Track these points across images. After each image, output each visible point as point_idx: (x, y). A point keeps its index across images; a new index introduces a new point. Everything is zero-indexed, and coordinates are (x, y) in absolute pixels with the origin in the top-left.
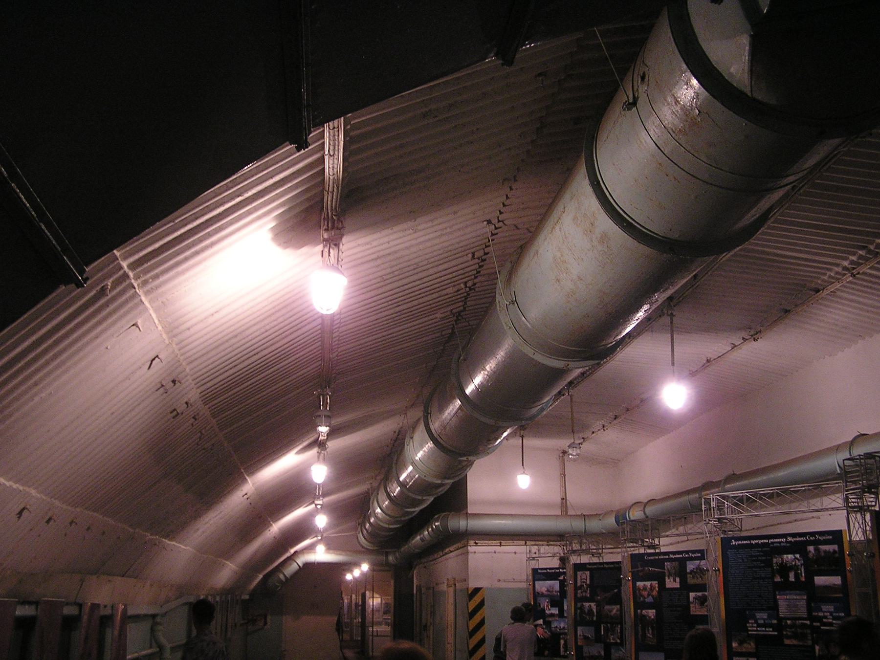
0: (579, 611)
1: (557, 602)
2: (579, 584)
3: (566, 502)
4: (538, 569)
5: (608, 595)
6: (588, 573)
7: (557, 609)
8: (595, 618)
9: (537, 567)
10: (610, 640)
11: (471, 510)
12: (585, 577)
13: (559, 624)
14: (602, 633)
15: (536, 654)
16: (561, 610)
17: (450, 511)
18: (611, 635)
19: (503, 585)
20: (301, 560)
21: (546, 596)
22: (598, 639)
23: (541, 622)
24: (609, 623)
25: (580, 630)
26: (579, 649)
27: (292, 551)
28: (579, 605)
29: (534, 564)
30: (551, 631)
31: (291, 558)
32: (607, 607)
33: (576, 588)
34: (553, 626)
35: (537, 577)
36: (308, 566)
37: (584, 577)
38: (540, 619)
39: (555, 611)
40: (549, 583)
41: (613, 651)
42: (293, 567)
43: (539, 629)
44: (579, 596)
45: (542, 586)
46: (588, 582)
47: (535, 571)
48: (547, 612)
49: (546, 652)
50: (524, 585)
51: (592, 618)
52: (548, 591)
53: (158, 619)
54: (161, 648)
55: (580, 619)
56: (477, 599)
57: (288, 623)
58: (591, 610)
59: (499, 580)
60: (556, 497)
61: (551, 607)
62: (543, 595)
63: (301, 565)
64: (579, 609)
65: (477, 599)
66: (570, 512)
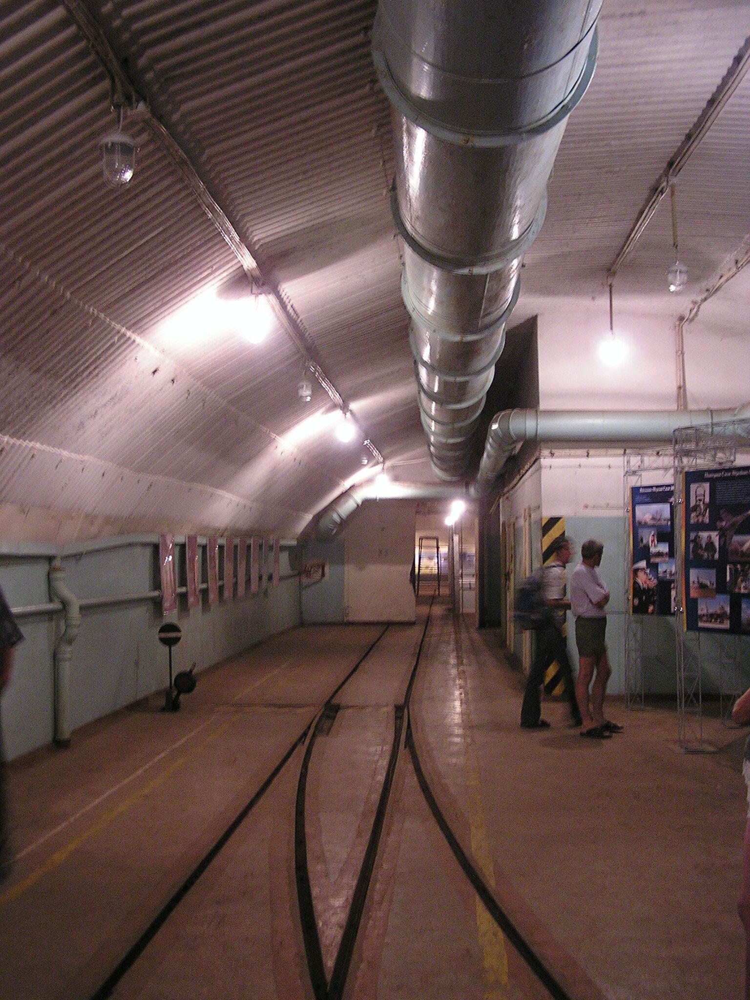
0: (692, 545)
1: (665, 535)
2: (693, 503)
3: (685, 390)
4: (640, 488)
5: (739, 519)
6: (707, 486)
7: (667, 545)
8: (717, 556)
9: (638, 485)
10: (740, 589)
11: (543, 405)
12: (702, 491)
13: (668, 567)
14: (728, 578)
15: (636, 610)
16: (671, 547)
17: (513, 408)
18: (742, 581)
19: (590, 513)
20: (359, 496)
21: (652, 526)
22: (722, 587)
23: (643, 564)
24: (739, 563)
25: (694, 574)
26: (692, 605)
27: (346, 484)
28: (692, 536)
29: (634, 481)
30: (658, 578)
31: (345, 494)
32: (737, 538)
33: (688, 510)
34: (660, 569)
35: (638, 498)
36: (368, 504)
37: (700, 491)
38: (641, 560)
39: (664, 548)
40: (655, 507)
41: (744, 606)
42: (348, 507)
43: (641, 575)
44: (692, 521)
45: (646, 512)
46: (707, 500)
47: (635, 491)
48: (653, 550)
49: (651, 608)
50: (620, 513)
51: (713, 556)
52: (653, 519)
53: (57, 563)
54: (65, 604)
55: (693, 560)
56: (554, 533)
57: (350, 572)
58: (710, 544)
59: (586, 507)
60: (670, 385)
61: (658, 541)
62: (645, 525)
63: (360, 502)
64: (692, 541)
65: (554, 533)
66: (691, 406)
